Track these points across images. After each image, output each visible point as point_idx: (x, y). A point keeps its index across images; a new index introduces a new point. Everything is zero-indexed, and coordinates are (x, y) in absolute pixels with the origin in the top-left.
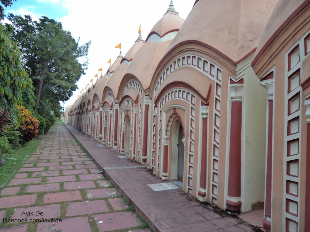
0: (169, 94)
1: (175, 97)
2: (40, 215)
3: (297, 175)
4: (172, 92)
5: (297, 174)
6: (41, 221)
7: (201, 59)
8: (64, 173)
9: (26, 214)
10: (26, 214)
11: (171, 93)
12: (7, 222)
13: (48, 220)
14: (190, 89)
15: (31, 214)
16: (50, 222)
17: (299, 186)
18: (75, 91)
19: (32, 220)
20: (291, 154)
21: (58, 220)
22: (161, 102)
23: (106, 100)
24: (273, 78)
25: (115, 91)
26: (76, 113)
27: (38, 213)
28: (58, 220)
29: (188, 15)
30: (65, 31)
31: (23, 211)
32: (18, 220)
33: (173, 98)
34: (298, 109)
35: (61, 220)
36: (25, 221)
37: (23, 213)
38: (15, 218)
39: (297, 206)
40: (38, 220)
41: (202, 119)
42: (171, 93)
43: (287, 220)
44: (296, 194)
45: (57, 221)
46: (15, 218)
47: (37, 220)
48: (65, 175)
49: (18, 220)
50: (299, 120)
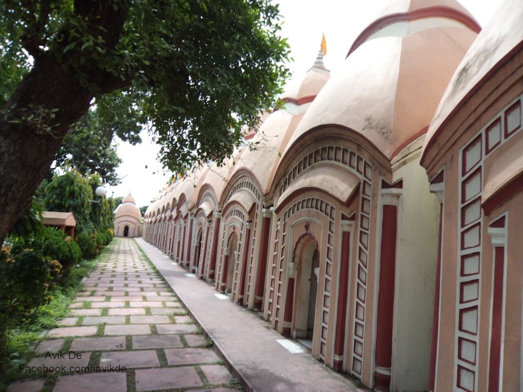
0: (299, 203)
2: (76, 357)
3: (474, 362)
5: (474, 359)
8: (143, 312)
16: (57, 357)
17: (483, 176)
18: (117, 168)
20: (465, 247)
24: (442, 181)
29: (321, 91)
34: (479, 217)
35: (81, 356)
36: (62, 369)
38: (44, 366)
39: (473, 376)
41: (342, 233)
42: (329, 246)
43: (460, 368)
44: (472, 361)
46: (44, 366)
48: (133, 308)
50: (481, 140)
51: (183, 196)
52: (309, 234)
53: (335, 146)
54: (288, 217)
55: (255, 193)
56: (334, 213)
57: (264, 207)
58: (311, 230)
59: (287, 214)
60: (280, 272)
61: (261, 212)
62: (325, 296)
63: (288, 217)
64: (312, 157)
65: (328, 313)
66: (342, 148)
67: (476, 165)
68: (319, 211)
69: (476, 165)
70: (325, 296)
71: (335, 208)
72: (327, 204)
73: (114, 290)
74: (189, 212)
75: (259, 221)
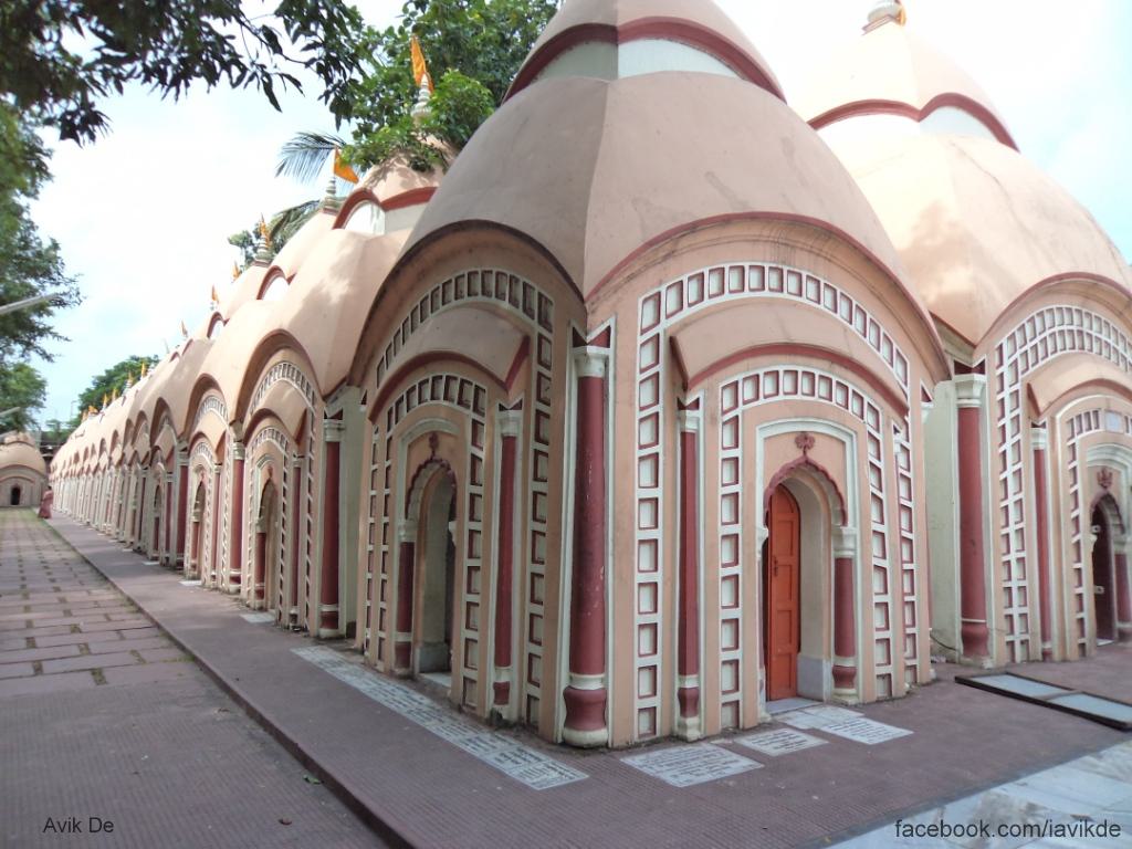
0: (399, 403)
1: (433, 398)
4: (436, 379)
6: (1042, 829)
7: (517, 281)
9: (58, 829)
10: (58, 829)
11: (430, 381)
12: (1064, 835)
13: (1067, 828)
14: (906, 115)
15: (1086, 830)
19: (924, 826)
21: (1105, 826)
22: (390, 413)
23: (157, 443)
25: (230, 385)
26: (93, 468)
27: (96, 825)
28: (1105, 826)
30: (43, 237)
31: (50, 819)
32: (965, 834)
33: (426, 401)
36: (982, 830)
37: (50, 824)
40: (1028, 829)
45: (1101, 830)
47: (1105, 835)
49: (965, 834)
51: (161, 405)
52: (437, 461)
53: (479, 270)
54: (397, 422)
55: (305, 389)
56: (484, 400)
57: (326, 418)
58: (442, 453)
59: (394, 416)
60: (384, 553)
61: (320, 434)
62: (467, 640)
63: (397, 422)
64: (437, 296)
65: (476, 641)
66: (474, 383)
67: (143, 494)
68: (455, 406)
69: (143, 494)
70: (467, 640)
71: (485, 387)
72: (525, 285)
73: (68, 628)
74: (321, 407)
75: (318, 456)
